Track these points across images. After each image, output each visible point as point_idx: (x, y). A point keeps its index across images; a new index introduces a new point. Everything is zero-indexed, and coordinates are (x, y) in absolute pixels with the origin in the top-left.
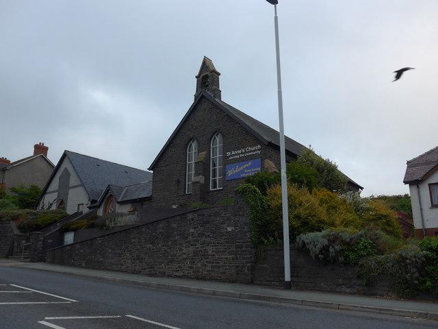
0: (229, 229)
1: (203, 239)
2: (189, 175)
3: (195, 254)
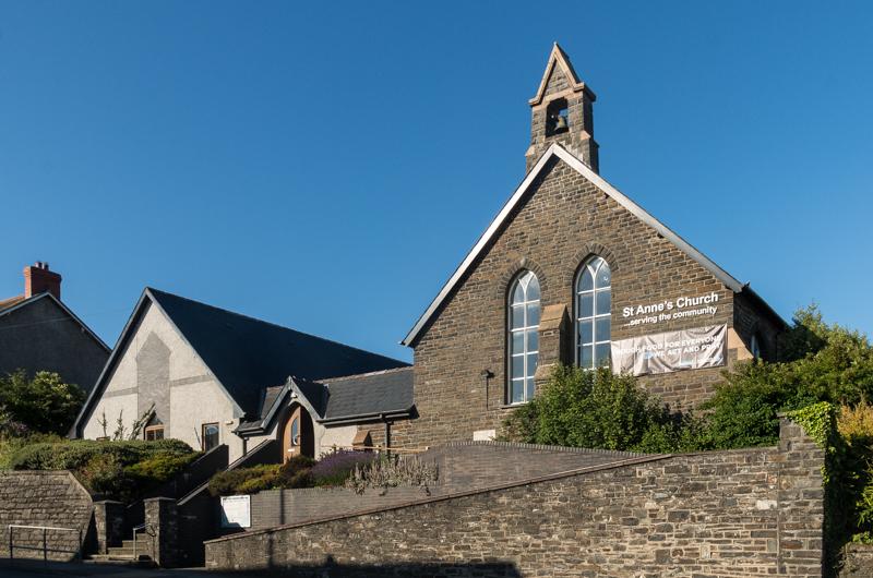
0: (763, 505)
1: (686, 524)
3: (661, 557)
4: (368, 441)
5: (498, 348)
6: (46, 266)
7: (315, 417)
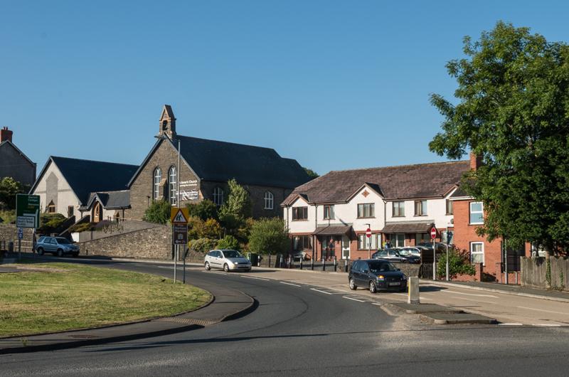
4: (118, 215)
7: (103, 207)
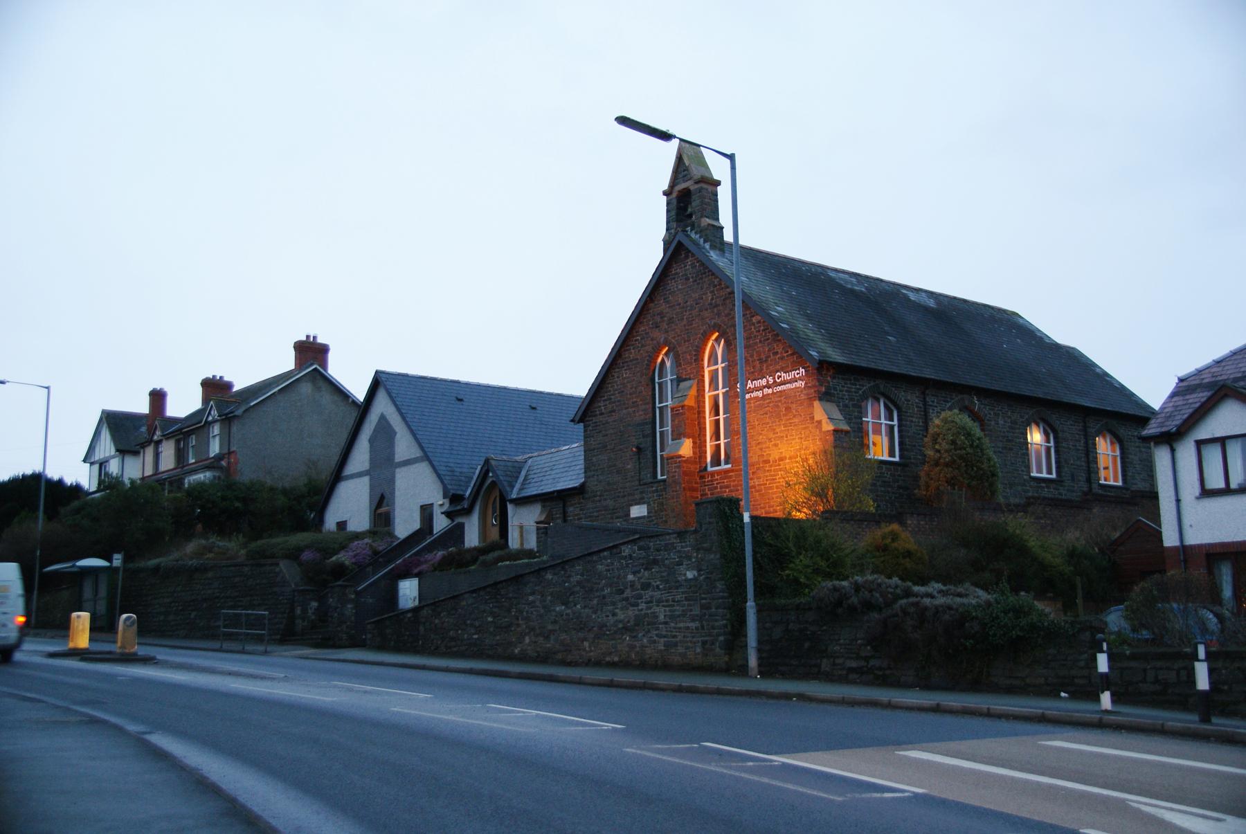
0: (690, 575)
1: (649, 593)
2: (662, 433)
5: (646, 423)
6: (315, 338)
